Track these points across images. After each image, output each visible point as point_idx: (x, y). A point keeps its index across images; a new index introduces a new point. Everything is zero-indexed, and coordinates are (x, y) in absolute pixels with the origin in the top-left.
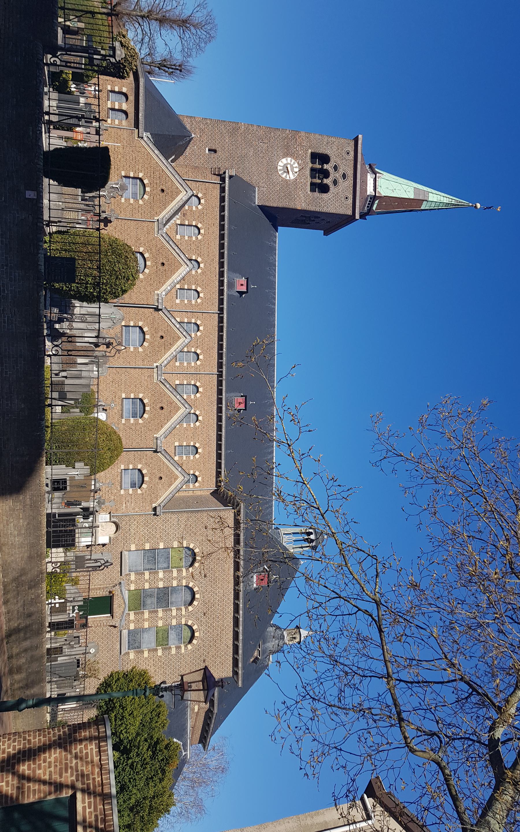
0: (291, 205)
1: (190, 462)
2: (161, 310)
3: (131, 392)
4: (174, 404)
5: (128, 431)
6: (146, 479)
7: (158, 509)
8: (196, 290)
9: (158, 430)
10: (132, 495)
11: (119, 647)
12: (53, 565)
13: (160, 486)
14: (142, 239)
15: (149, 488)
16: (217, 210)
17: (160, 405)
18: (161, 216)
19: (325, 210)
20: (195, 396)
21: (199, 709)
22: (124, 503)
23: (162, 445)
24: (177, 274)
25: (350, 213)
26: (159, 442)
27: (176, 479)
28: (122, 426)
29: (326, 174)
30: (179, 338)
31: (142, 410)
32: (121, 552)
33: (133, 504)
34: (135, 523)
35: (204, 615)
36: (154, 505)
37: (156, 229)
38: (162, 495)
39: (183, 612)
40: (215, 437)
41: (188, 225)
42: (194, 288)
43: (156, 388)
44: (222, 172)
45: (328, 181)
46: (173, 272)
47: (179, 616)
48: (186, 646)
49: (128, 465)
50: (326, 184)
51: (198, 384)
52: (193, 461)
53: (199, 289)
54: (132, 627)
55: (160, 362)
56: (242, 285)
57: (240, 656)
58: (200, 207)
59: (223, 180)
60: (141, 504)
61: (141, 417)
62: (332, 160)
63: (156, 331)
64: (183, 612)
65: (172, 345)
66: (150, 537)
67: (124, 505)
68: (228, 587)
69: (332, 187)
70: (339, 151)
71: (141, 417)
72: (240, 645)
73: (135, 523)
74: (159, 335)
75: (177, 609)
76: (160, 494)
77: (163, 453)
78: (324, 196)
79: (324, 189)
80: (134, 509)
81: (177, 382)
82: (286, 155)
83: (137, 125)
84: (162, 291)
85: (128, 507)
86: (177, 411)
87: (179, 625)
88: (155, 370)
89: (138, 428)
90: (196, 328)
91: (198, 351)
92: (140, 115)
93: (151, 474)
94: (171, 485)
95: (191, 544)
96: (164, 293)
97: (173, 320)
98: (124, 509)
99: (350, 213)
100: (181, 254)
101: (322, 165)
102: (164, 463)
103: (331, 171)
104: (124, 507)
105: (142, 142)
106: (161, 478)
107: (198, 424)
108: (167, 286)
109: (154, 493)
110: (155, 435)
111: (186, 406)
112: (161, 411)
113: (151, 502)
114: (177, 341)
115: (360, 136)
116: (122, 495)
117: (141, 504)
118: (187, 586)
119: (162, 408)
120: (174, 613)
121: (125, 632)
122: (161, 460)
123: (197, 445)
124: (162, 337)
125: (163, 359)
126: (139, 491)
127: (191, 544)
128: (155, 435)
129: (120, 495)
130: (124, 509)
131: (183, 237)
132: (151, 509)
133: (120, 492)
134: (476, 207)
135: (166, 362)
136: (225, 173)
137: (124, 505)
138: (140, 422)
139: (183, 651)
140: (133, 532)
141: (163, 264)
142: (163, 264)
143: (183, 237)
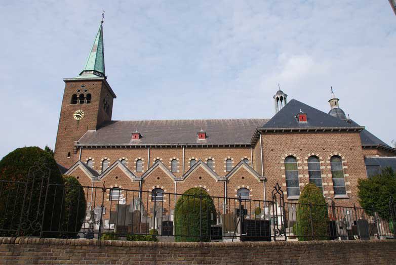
2: (142, 179)
6: (243, 186)
7: (262, 179)
8: (88, 161)
11: (345, 200)
12: (277, 235)
13: (248, 178)
16: (133, 150)
17: (198, 179)
18: (91, 179)
20: (233, 161)
21: (378, 155)
23: (223, 177)
24: (122, 170)
25: (101, 83)
26: (221, 179)
27: (243, 169)
29: (82, 96)
30: (159, 168)
31: (244, 190)
35: (324, 149)
37: (97, 181)
39: (323, 162)
41: (102, 166)
42: (135, 163)
44: (75, 148)
46: (121, 172)
47: (302, 165)
48: (343, 160)
51: (190, 159)
52: (235, 161)
53: (136, 160)
54: (332, 192)
55: (172, 179)
57: (333, 128)
58: (109, 159)
61: (248, 190)
64: (323, 162)
71: (248, 190)
72: (341, 128)
74: (157, 180)
75: (322, 166)
77: (227, 177)
79: (89, 96)
81: (225, 171)
82: (72, 116)
84: (132, 178)
86: (202, 169)
87: (331, 164)
88: (178, 182)
90: (140, 161)
91: (171, 159)
96: (133, 177)
97: (148, 172)
99: (101, 83)
101: (77, 98)
102: (234, 176)
103: (80, 93)
107: (213, 159)
108: (129, 175)
109: (252, 181)
111: (199, 163)
112: (202, 178)
114: (160, 169)
118: (308, 160)
119: (200, 178)
120: (324, 167)
121: (337, 196)
123: (226, 159)
125: (171, 177)
126: (251, 190)
131: (143, 169)
135: (173, 176)
136: (76, 146)
139: (346, 162)
141: (117, 178)
142: (117, 178)
143: (143, 169)
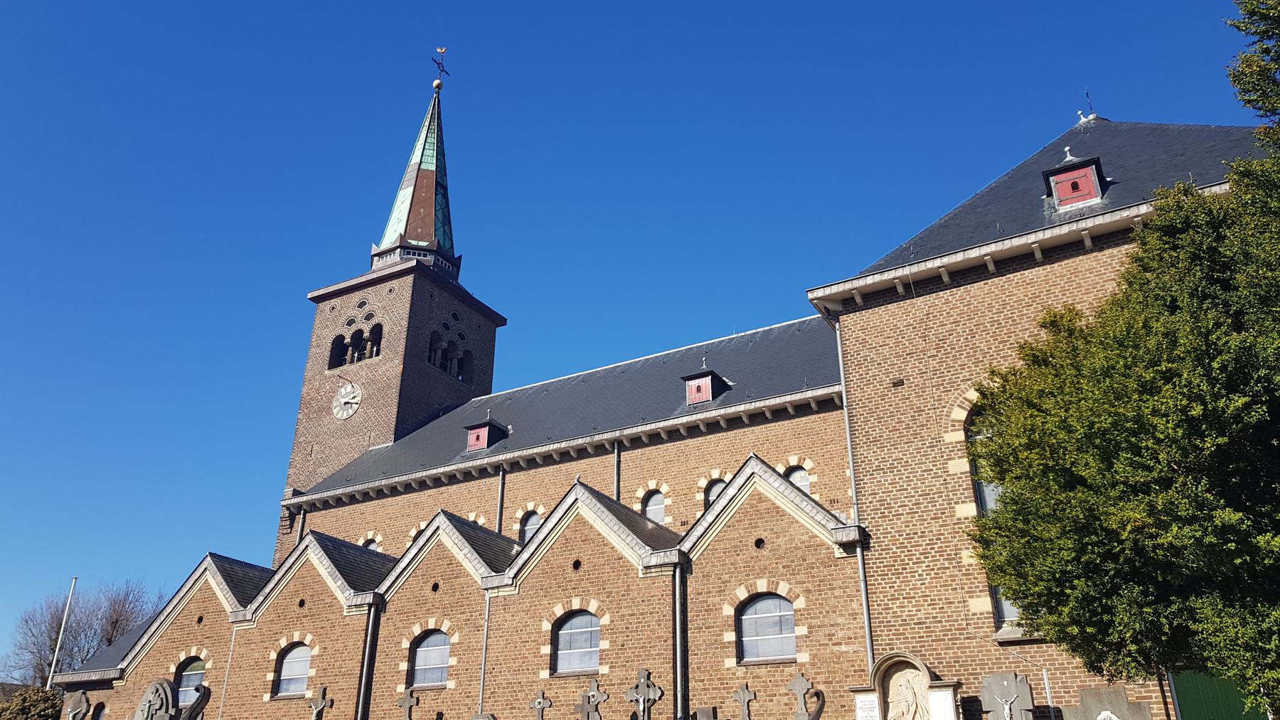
0: (397, 382)
1: (826, 479)
3: (537, 654)
4: (568, 533)
5: (629, 653)
9: (630, 568)
10: (810, 627)
13: (781, 541)
14: (257, 655)
15: (790, 572)
19: (405, 323)
22: (836, 648)
28: (617, 671)
32: (1002, 644)
33: (840, 620)
34: (895, 606)
36: (839, 553)
38: (808, 532)
40: (757, 429)
43: (532, 588)
45: (367, 328)
49: (724, 645)
50: (371, 331)
56: (478, 438)
59: (299, 507)
60: (837, 593)
62: (339, 331)
63: (422, 602)
65: (452, 561)
66: (941, 552)
67: (843, 648)
68: (1090, 270)
69: (374, 321)
70: (332, 322)
73: (895, 606)
76: (805, 538)
78: (385, 330)
79: (377, 331)
80: (854, 616)
83: (106, 684)
85: (850, 633)
86: (585, 523)
89: (621, 625)
92: (94, 678)
93: (753, 571)
94: (778, 510)
95: (953, 416)
98: (855, 647)
100: (287, 565)
103: (354, 328)
104: (850, 648)
105: (129, 670)
106: (759, 543)
110: (641, 575)
113: (831, 562)
115: (310, 296)
116: (813, 656)
117: (837, 593)
122: (711, 549)
124: (435, 587)
127: (953, 416)
128: (641, 575)
129: (813, 664)
130: (855, 647)
132: (852, 560)
133: (803, 665)
134: (439, 86)
137: (843, 648)
138: (608, 622)
140: (926, 609)
